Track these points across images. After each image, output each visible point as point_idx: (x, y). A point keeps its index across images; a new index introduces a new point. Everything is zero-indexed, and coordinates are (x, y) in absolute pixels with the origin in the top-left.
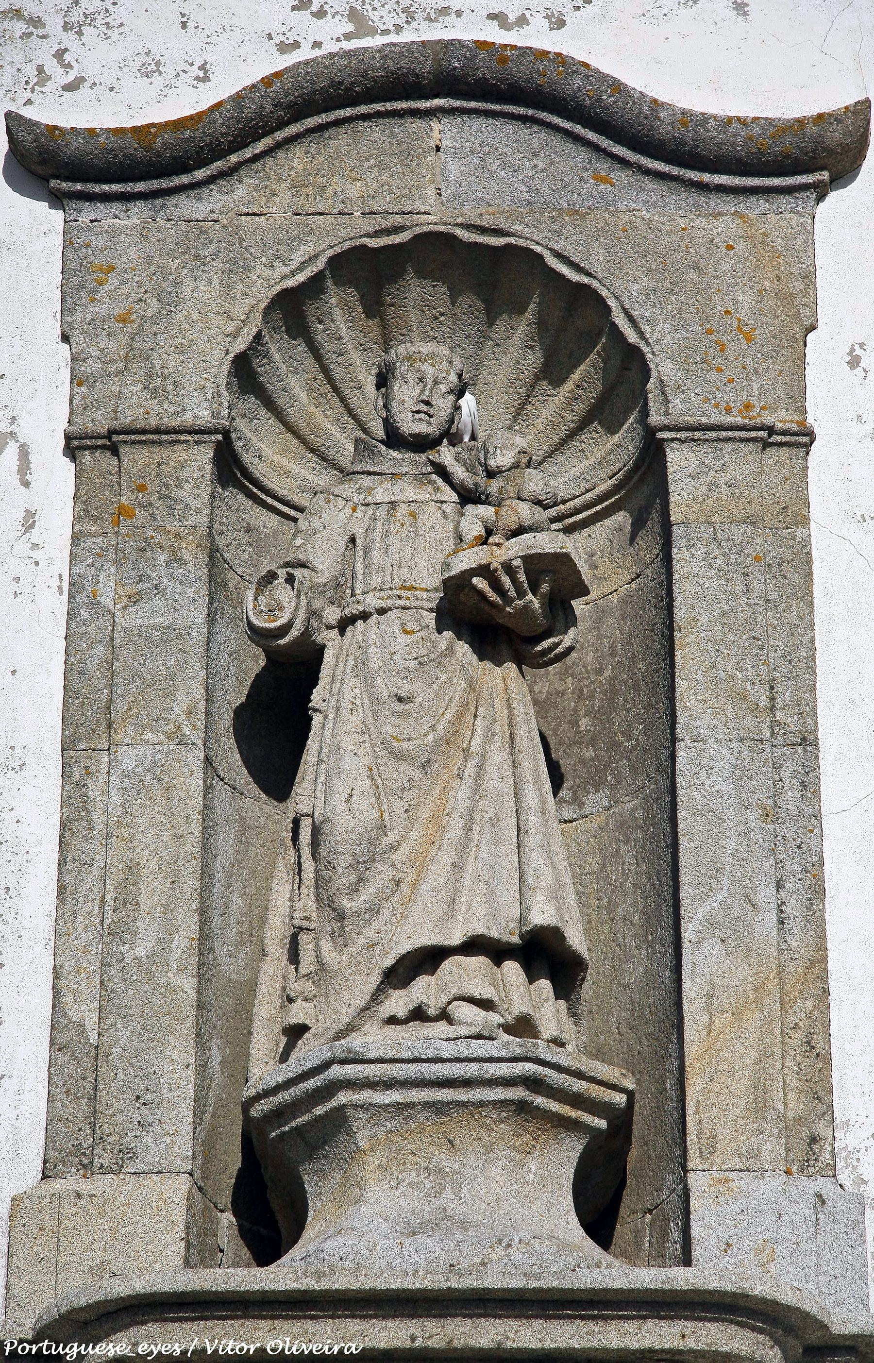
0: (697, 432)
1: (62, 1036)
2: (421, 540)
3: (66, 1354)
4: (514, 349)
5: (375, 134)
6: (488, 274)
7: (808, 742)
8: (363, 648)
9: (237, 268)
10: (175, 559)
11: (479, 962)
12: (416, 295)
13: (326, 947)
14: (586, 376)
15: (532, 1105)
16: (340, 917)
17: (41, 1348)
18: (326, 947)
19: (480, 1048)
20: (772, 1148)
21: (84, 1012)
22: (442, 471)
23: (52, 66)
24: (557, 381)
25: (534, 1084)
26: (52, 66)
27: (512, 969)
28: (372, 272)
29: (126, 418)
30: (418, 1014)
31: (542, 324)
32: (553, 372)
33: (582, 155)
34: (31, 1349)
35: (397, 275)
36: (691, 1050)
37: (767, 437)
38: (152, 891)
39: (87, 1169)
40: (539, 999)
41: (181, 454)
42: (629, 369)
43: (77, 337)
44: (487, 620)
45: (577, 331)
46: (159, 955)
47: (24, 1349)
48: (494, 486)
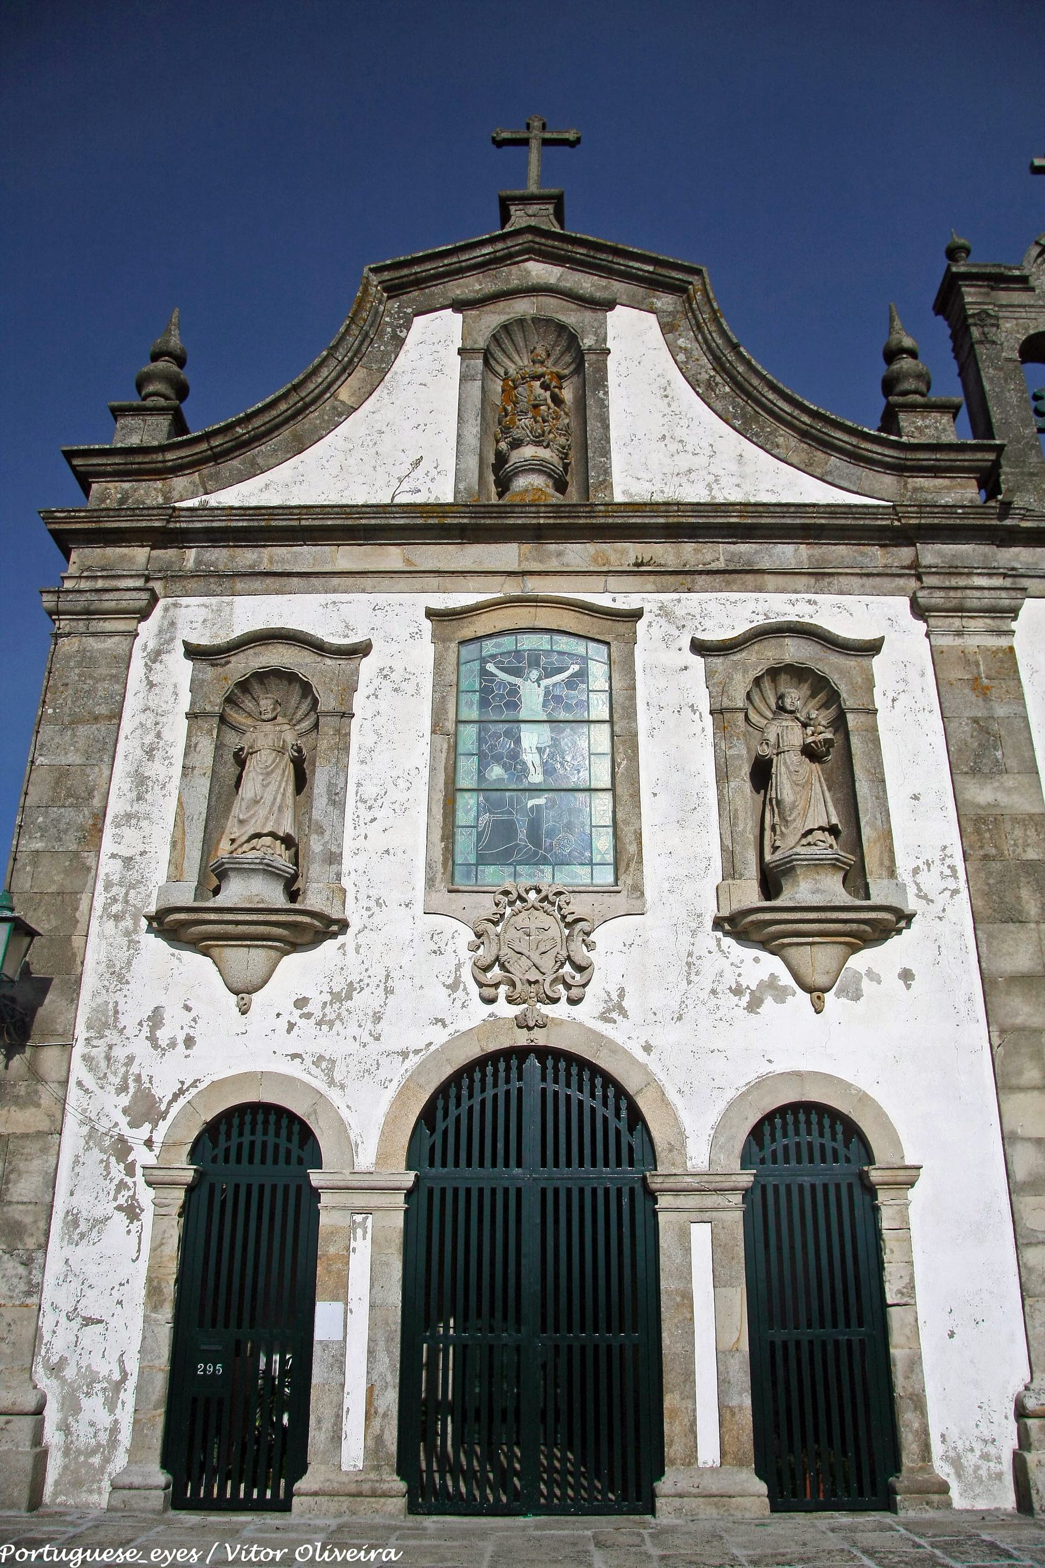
0: (853, 710)
1: (723, 848)
2: (795, 736)
4: (805, 689)
5: (773, 641)
6: (799, 673)
7: (883, 781)
8: (785, 759)
9: (745, 671)
10: (738, 739)
11: (820, 832)
12: (783, 678)
13: (783, 828)
14: (822, 697)
15: (835, 865)
16: (787, 821)
18: (783, 828)
19: (825, 852)
20: (885, 873)
21: (728, 842)
22: (797, 719)
23: (699, 626)
24: (814, 698)
25: (837, 859)
26: (699, 626)
27: (826, 833)
28: (774, 673)
29: (724, 706)
30: (809, 844)
31: (812, 685)
32: (813, 696)
33: (820, 647)
35: (779, 674)
36: (865, 851)
37: (343, 715)
38: (741, 815)
39: (734, 878)
40: (831, 840)
41: (737, 714)
42: (315, 702)
43: (711, 688)
44: (810, 752)
45: (822, 687)
46: (745, 830)
48: (812, 722)
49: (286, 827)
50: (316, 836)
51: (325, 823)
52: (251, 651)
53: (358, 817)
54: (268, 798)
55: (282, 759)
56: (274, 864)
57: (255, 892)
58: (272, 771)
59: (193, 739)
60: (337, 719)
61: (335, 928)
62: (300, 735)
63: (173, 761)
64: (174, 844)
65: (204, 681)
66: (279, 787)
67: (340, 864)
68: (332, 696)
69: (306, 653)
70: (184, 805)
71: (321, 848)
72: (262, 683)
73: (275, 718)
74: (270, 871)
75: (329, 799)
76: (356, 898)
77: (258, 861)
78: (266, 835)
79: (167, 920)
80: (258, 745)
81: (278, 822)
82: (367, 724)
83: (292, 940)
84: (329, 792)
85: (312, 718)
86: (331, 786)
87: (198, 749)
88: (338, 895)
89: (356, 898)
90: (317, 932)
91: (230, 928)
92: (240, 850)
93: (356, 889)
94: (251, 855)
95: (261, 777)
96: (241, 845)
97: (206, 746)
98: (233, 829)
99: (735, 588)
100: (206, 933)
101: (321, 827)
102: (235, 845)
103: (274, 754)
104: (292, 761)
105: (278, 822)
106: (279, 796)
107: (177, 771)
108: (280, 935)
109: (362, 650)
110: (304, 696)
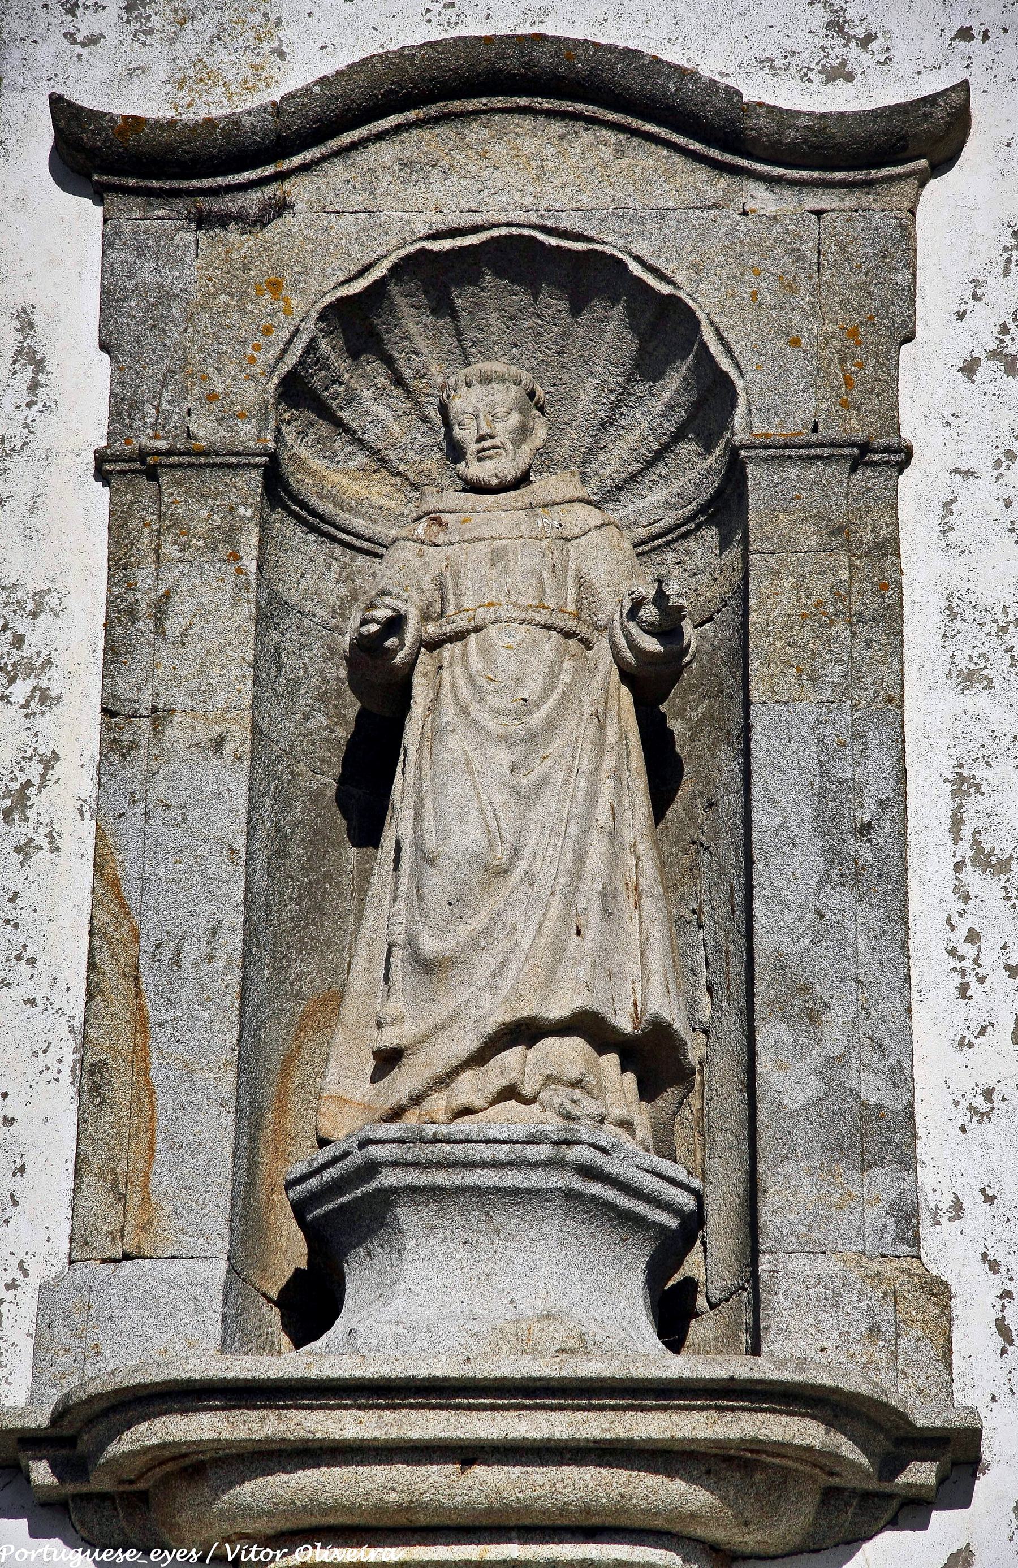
3: (69, 1561)
14: (673, 384)
17: (39, 1556)
28: (439, 274)
34: (29, 1556)
42: (713, 398)
47: (21, 1555)
49: (646, 991)
50: (785, 1034)
51: (820, 967)
52: (386, 153)
53: (973, 937)
54: (545, 852)
55: (585, 671)
56: (613, 1166)
57: (529, 1305)
58: (550, 726)
59: (144, 576)
60: (836, 471)
61: (921, 1474)
62: (649, 547)
63: (53, 682)
64: (93, 1080)
65: (166, 297)
66: (592, 799)
67: (908, 1162)
68: (798, 364)
69: (649, 159)
70: (132, 891)
71: (814, 1086)
72: (442, 306)
73: (522, 480)
74: (597, 1201)
75: (833, 856)
76: (1003, 1329)
77: (543, 1152)
78: (563, 1028)
79: (114, 1449)
80: (471, 597)
81: (606, 970)
82: (979, 497)
83: (718, 1534)
84: (825, 820)
85: (694, 471)
86: (829, 792)
87: (173, 626)
88: (920, 1310)
89: (1003, 1329)
90: (832, 1496)
91: (435, 1483)
92: (439, 1104)
93: (997, 1283)
94: (509, 1120)
95: (504, 757)
96: (444, 1080)
97: (210, 608)
98: (379, 1006)
99: (803, 121)
100: (293, 1509)
101: (805, 989)
102: (403, 1083)
103: (550, 644)
104: (627, 676)
105: (606, 970)
106: (597, 845)
107: (76, 730)
108: (675, 1513)
109: (926, 137)
110: (648, 367)
